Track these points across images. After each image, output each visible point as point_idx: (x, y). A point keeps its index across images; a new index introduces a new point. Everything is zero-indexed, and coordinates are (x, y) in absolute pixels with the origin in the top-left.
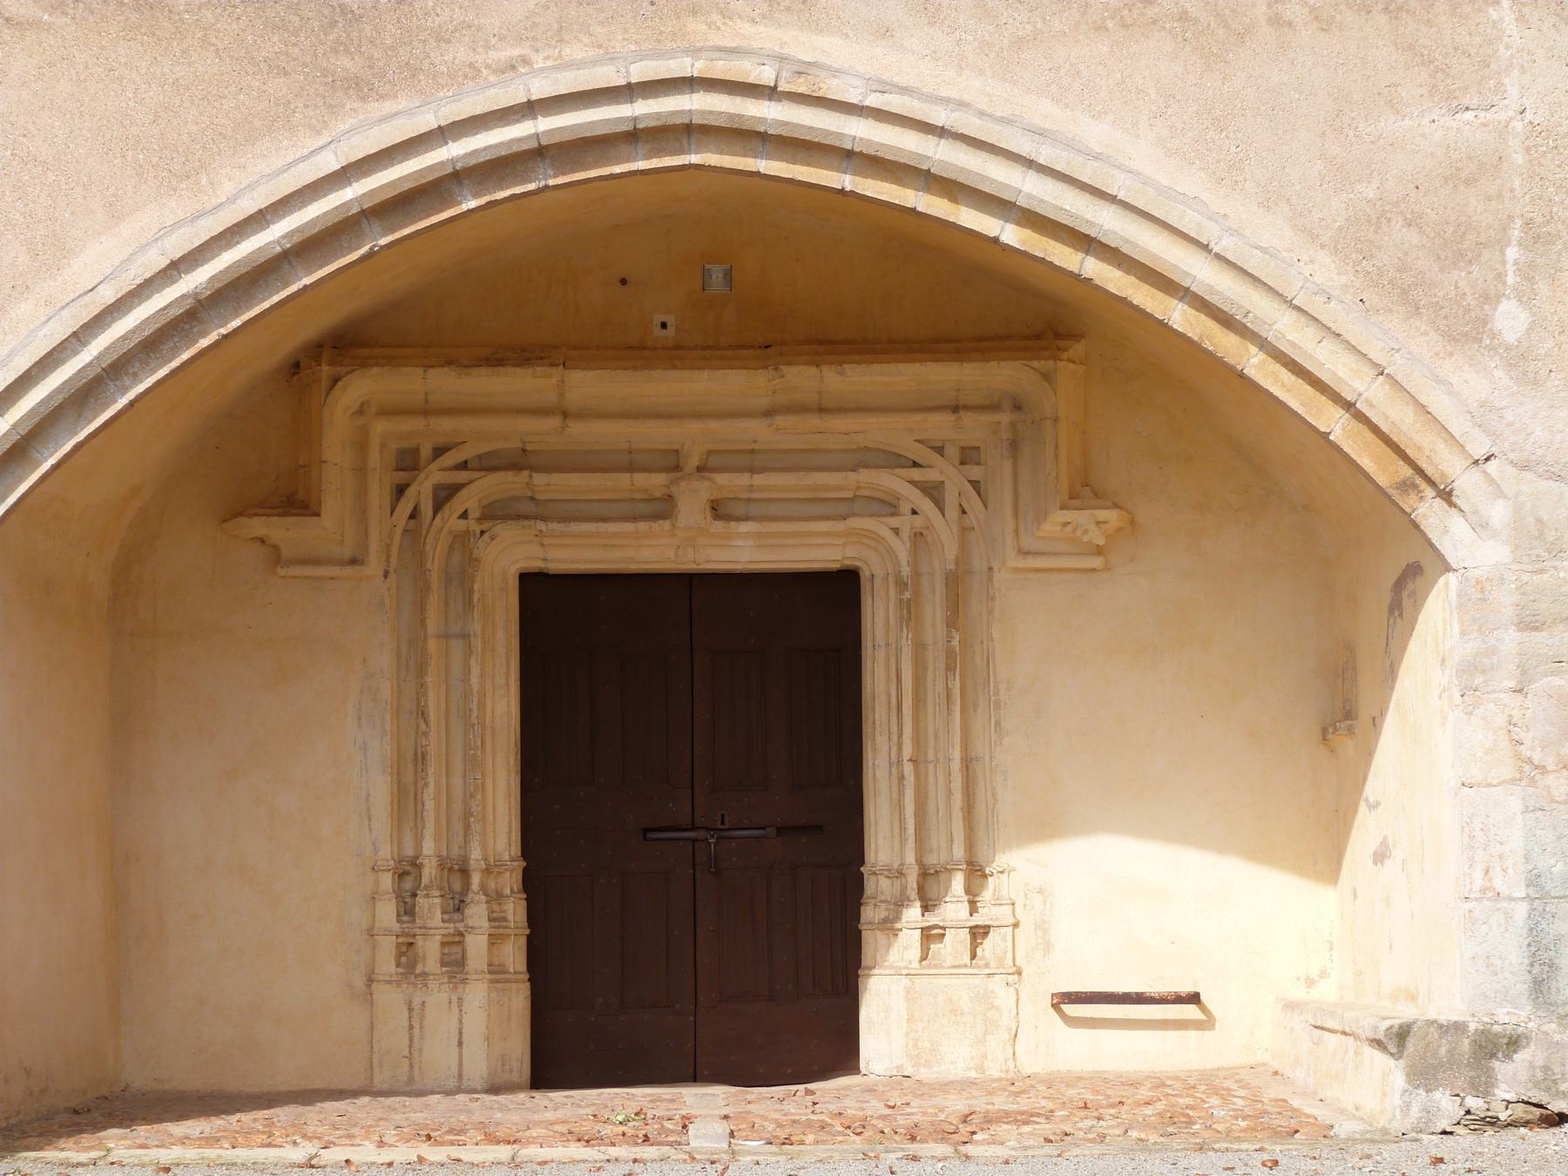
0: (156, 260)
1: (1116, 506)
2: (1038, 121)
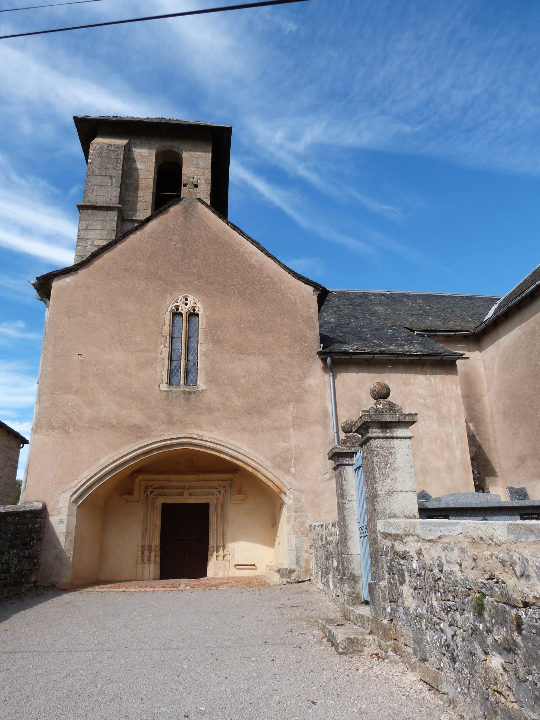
0: (112, 461)
1: (244, 494)
2: (231, 443)
